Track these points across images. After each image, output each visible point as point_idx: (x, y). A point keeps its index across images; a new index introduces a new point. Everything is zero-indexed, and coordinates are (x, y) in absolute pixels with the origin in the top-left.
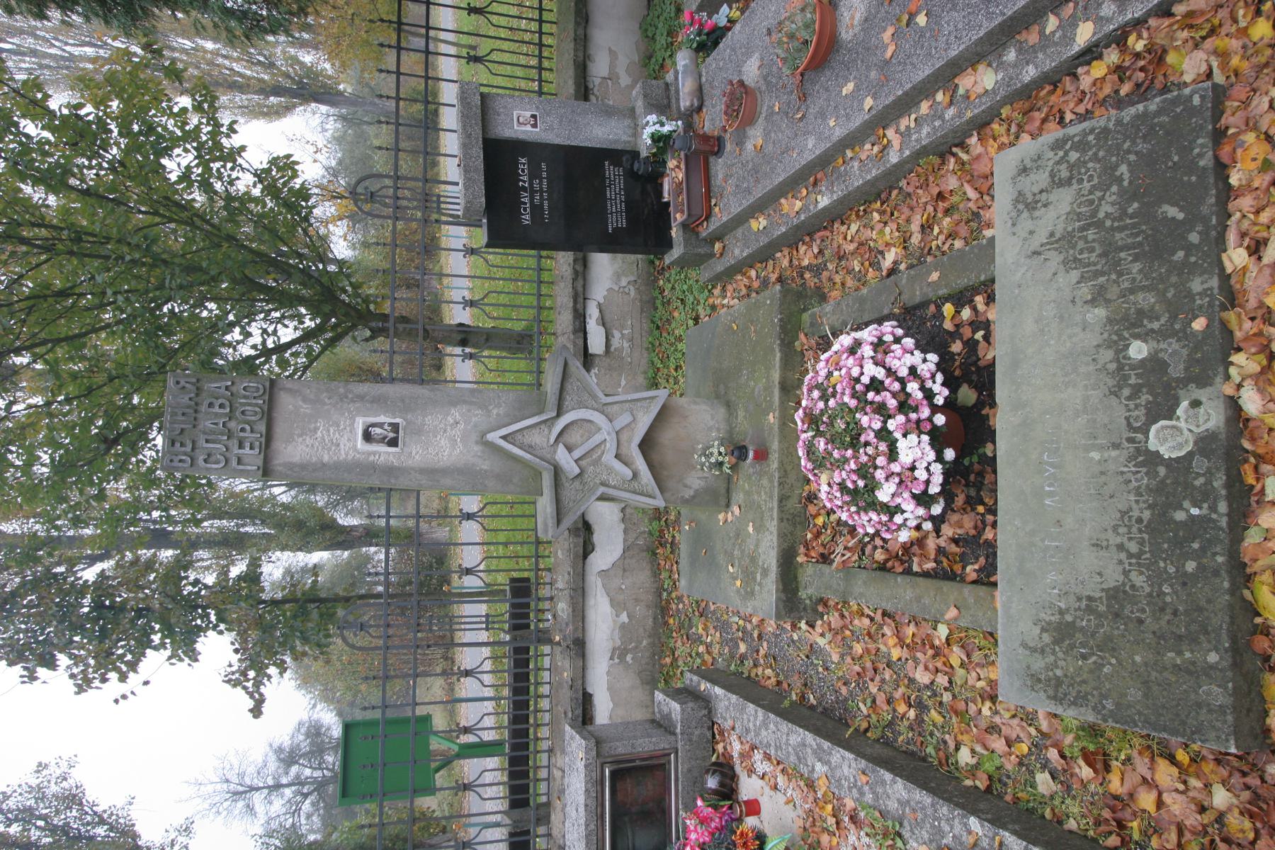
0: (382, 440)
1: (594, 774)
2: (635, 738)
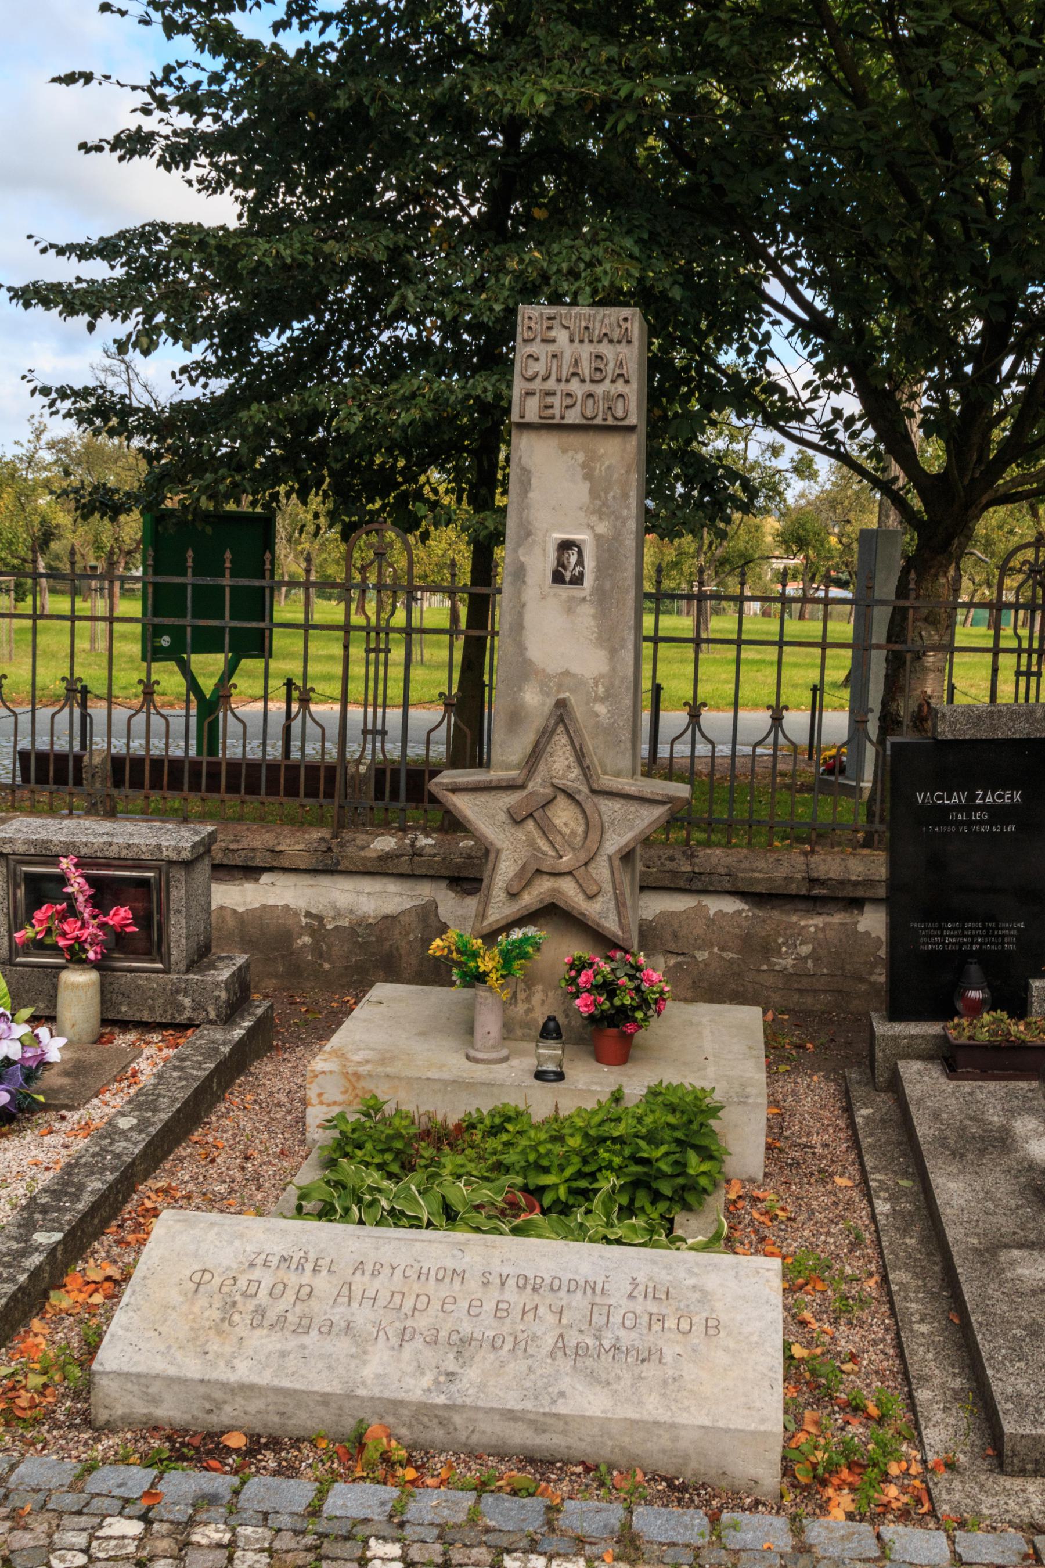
0: (561, 564)
1: (147, 856)
2: (188, 917)
